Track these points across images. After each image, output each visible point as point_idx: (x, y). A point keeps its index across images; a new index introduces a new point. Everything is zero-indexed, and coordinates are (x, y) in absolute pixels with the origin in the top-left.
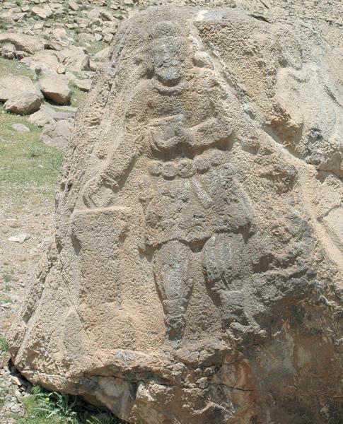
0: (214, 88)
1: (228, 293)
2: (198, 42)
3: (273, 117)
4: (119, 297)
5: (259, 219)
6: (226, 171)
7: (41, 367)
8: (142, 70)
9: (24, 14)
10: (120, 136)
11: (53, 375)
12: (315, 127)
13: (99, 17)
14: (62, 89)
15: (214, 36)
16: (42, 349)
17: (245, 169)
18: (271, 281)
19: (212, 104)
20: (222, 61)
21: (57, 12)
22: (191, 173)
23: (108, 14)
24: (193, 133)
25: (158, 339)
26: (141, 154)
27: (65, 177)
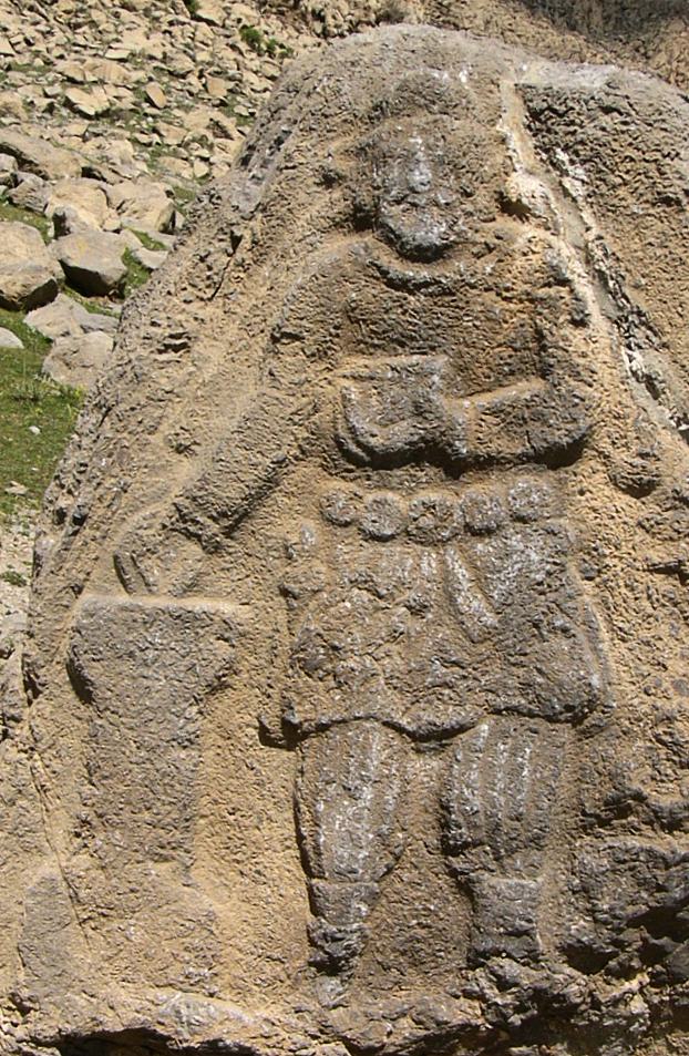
0: (552, 291)
1: (501, 883)
2: (521, 145)
4: (187, 851)
5: (626, 694)
6: (551, 541)
8: (341, 206)
9: (49, 101)
10: (247, 394)
13: (208, 127)
14: (108, 266)
15: (574, 133)
19: (539, 335)
20: (587, 215)
21: (119, 104)
22: (446, 534)
23: (229, 123)
24: (465, 415)
25: (283, 976)
27: (70, 492)
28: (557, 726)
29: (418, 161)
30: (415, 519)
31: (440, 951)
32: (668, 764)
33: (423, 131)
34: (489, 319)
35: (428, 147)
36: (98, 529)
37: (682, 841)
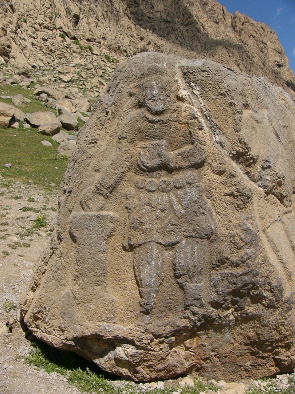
0: (193, 121)
1: (191, 285)
2: (181, 82)
3: (238, 148)
4: (105, 282)
5: (222, 230)
6: (198, 189)
7: (42, 329)
8: (135, 102)
10: (113, 154)
11: (52, 336)
12: (267, 159)
13: (98, 83)
14: (73, 122)
15: (195, 78)
16: (44, 316)
17: (213, 188)
18: (224, 277)
21: (74, 78)
22: (169, 189)
23: (103, 81)
27: (67, 184)
29: (154, 88)
30: (161, 186)
31: (176, 306)
32: (234, 249)
33: (155, 80)
36: (75, 194)
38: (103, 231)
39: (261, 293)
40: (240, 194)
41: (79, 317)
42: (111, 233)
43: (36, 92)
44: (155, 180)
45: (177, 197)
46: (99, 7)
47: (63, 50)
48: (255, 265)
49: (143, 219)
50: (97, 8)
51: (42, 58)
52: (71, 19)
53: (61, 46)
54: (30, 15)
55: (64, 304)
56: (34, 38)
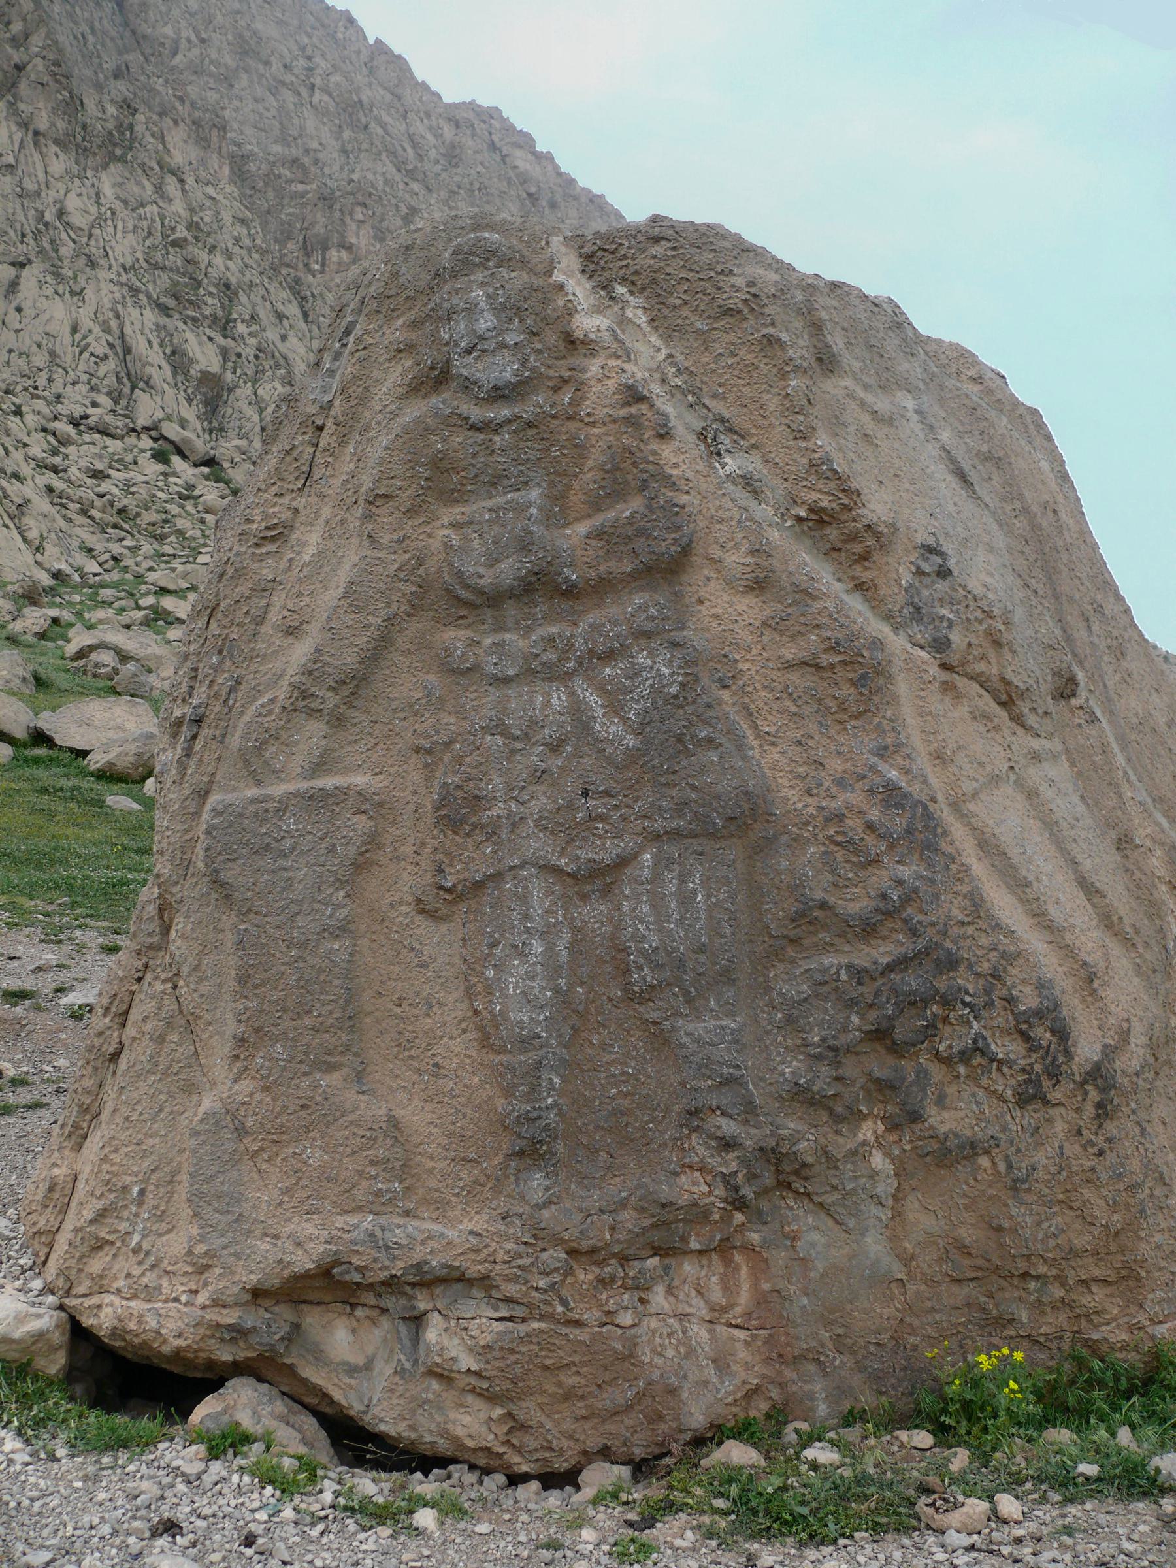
0: (633, 410)
1: (700, 1028)
2: (580, 290)
3: (815, 496)
4: (356, 1054)
12: (931, 541)
15: (627, 266)
22: (571, 665)
25: (483, 1179)
26: (414, 610)
28: (723, 843)
29: (482, 311)
30: (537, 655)
31: (648, 1122)
32: (848, 866)
33: (482, 285)
34: (576, 446)
35: (489, 296)
36: (216, 727)
37: (881, 950)
38: (332, 850)
39: (981, 1044)
40: (840, 658)
41: (264, 1206)
42: (362, 854)
43: (71, 649)
44: (515, 637)
45: (602, 690)
46: (293, 341)
47: (168, 506)
48: (940, 927)
49: (483, 784)
50: (288, 344)
51: (92, 540)
52: (190, 391)
53: (160, 494)
54: (36, 388)
55: (201, 1159)
56: (55, 470)
